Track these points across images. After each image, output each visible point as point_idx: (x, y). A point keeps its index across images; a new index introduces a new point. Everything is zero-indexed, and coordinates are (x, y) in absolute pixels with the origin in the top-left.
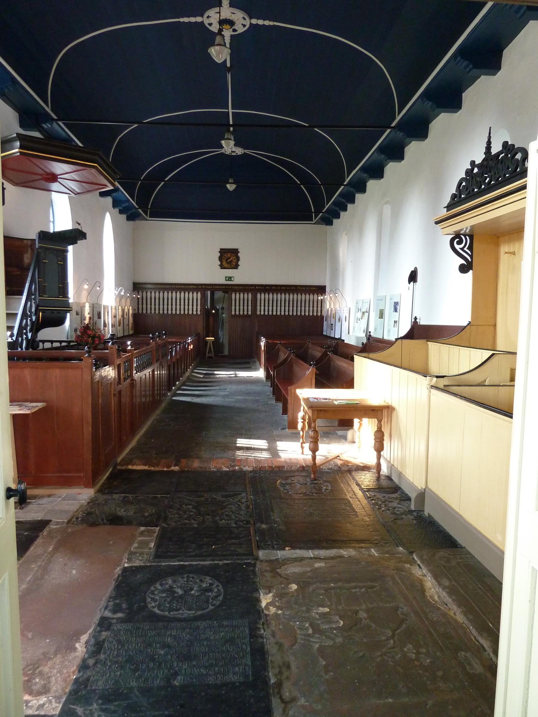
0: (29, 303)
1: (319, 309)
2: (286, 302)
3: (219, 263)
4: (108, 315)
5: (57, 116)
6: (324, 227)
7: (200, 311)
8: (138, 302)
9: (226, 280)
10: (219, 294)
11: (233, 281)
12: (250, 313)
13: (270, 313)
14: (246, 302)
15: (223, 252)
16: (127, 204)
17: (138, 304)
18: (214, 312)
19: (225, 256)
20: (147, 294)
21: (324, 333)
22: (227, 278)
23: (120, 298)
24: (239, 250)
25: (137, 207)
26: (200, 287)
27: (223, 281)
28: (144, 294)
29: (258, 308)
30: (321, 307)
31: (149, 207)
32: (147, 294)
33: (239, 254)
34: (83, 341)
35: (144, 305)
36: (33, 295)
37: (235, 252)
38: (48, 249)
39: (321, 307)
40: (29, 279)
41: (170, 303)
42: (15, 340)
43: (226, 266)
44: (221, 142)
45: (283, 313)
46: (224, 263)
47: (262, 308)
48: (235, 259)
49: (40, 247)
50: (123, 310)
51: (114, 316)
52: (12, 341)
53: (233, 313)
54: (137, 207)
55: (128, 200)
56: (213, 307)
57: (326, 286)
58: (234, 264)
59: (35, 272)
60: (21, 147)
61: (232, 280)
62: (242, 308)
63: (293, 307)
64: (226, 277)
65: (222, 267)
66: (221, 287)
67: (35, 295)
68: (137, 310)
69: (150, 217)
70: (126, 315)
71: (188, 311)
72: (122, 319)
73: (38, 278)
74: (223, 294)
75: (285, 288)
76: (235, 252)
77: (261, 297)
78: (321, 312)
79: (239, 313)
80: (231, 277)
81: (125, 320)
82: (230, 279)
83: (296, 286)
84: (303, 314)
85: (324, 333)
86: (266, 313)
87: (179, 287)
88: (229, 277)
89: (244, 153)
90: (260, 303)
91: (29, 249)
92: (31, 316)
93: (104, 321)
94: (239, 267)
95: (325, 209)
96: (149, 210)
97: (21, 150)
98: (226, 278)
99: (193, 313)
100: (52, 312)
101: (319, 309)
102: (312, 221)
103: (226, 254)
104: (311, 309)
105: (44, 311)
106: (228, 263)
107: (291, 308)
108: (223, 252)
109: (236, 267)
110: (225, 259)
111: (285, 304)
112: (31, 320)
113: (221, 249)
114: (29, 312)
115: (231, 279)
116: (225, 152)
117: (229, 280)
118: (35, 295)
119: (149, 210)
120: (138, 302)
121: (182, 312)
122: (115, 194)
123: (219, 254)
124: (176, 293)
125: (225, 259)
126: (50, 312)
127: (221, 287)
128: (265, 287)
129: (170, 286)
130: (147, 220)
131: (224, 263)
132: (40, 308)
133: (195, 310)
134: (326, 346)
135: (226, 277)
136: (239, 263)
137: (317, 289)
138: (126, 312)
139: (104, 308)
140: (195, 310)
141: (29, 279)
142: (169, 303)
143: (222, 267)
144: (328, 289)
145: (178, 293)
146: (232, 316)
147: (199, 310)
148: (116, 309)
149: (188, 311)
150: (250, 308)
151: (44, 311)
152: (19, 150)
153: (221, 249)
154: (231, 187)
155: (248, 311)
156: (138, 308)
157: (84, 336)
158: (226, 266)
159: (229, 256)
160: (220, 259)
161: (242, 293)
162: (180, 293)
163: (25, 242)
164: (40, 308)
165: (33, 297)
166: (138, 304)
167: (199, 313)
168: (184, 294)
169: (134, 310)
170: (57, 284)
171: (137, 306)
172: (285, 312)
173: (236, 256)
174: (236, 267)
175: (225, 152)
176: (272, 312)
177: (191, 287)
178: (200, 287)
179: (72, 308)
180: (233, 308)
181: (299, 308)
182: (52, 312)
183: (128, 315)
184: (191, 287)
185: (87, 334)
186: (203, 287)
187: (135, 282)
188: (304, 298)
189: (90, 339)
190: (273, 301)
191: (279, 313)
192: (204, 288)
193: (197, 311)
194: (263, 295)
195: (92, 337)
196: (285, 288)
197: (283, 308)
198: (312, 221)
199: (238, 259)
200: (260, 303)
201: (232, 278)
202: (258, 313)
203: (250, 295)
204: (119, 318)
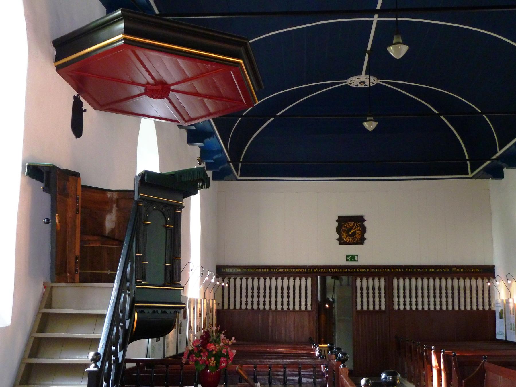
0: (123, 296)
1: (486, 300)
2: (485, 292)
3: (337, 236)
4: (194, 314)
5: (159, 10)
6: (491, 182)
7: (312, 305)
8: (223, 292)
9: (348, 260)
10: (329, 280)
11: (357, 261)
12: (383, 307)
13: (414, 308)
14: (377, 292)
15: (342, 221)
16: (220, 155)
17: (223, 296)
18: (327, 306)
19: (345, 226)
20: (235, 281)
21: (500, 336)
22: (349, 258)
23: (206, 286)
24: (365, 218)
25: (230, 160)
26: (311, 270)
27: (342, 262)
28: (232, 280)
29: (396, 300)
30: (489, 298)
31: (241, 160)
32: (235, 281)
33: (365, 224)
34: (200, 362)
35: (254, 297)
36: (128, 281)
37: (359, 220)
38: (152, 202)
39: (489, 298)
40: (124, 252)
41: (297, 295)
42: (100, 367)
43: (348, 240)
44: (388, 49)
45: (420, 308)
46: (344, 236)
47: (402, 300)
48: (359, 230)
49: (142, 199)
50: (208, 305)
51: (199, 313)
52: (96, 369)
53: (359, 308)
54: (230, 160)
55: (222, 151)
56: (325, 300)
57: (494, 266)
58: (358, 237)
59: (133, 241)
60: (127, 31)
61: (356, 259)
62: (371, 300)
63: (471, 298)
64: (347, 256)
65: (341, 241)
66: (341, 270)
67: (130, 281)
68: (221, 305)
69: (241, 176)
70: (211, 312)
71: (294, 304)
72: (206, 318)
73: (136, 253)
74: (333, 280)
75: (433, 270)
76: (359, 220)
77: (398, 283)
78: (490, 305)
79: (362, 308)
80: (354, 256)
81: (209, 320)
82: (352, 258)
83: (450, 267)
84: (481, 308)
85: (500, 336)
86: (468, 308)
87: (281, 270)
88: (352, 256)
89: (377, 83)
90: (398, 293)
91: (115, 205)
92: (123, 322)
93: (190, 322)
94: (366, 241)
95: (497, 155)
96: (240, 164)
97: (127, 36)
98: (347, 258)
99: (300, 308)
100: (154, 312)
101: (486, 300)
102: (467, 174)
103: (347, 224)
104: (474, 300)
105: (141, 310)
106: (349, 236)
107: (444, 300)
108: (342, 221)
109: (361, 241)
110: (345, 231)
111: (471, 293)
112: (123, 327)
113: (339, 217)
114: (121, 313)
115: (354, 258)
116: (351, 84)
117: (351, 260)
118: (130, 281)
119: (240, 164)
120: (223, 292)
121: (255, 307)
122: (208, 139)
123: (337, 224)
124: (253, 279)
125: (345, 231)
126: (151, 311)
127: (341, 270)
128: (404, 270)
129: (260, 270)
130: (237, 180)
131: (344, 236)
132: (136, 304)
133: (303, 303)
134: (485, 356)
135: (347, 256)
136: (366, 235)
137: (481, 270)
138: (211, 308)
139: (190, 302)
140: (303, 303)
141: (124, 252)
142: (248, 294)
143: (341, 241)
144: (498, 272)
145: (268, 280)
146: (358, 312)
147: (309, 304)
148: (201, 303)
149: (294, 304)
150: (383, 300)
151: (141, 310)
152: (124, 36)
153: (339, 217)
154: (370, 126)
155: (380, 305)
156: (223, 301)
157: (202, 354)
158: (348, 240)
159: (351, 225)
160: (339, 230)
161: (371, 278)
162: (253, 279)
163: (109, 194)
164: (136, 304)
165: (128, 284)
166: (223, 296)
167: (309, 308)
168: (288, 281)
169: (218, 304)
170: (163, 262)
171: (221, 299)
172: (429, 305)
173: (360, 226)
174: (361, 241)
175: (351, 84)
176: (417, 305)
177: (298, 270)
178: (311, 270)
179: (184, 304)
180: (359, 300)
181: (456, 300)
182: (154, 312)
183: (212, 312)
184: (298, 270)
185: (207, 350)
186: (315, 270)
187: (222, 263)
188: (403, 283)
189: (213, 359)
190: (441, 290)
191: (432, 308)
192: (316, 272)
193: (306, 305)
194: (365, 281)
195: (215, 354)
196: (433, 270)
197: (432, 300)
198: (467, 174)
199: (364, 230)
200: (398, 293)
201: (356, 257)
202: (396, 308)
203: (383, 281)
204: (204, 317)
